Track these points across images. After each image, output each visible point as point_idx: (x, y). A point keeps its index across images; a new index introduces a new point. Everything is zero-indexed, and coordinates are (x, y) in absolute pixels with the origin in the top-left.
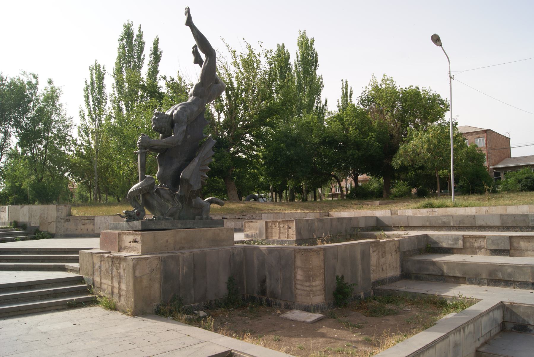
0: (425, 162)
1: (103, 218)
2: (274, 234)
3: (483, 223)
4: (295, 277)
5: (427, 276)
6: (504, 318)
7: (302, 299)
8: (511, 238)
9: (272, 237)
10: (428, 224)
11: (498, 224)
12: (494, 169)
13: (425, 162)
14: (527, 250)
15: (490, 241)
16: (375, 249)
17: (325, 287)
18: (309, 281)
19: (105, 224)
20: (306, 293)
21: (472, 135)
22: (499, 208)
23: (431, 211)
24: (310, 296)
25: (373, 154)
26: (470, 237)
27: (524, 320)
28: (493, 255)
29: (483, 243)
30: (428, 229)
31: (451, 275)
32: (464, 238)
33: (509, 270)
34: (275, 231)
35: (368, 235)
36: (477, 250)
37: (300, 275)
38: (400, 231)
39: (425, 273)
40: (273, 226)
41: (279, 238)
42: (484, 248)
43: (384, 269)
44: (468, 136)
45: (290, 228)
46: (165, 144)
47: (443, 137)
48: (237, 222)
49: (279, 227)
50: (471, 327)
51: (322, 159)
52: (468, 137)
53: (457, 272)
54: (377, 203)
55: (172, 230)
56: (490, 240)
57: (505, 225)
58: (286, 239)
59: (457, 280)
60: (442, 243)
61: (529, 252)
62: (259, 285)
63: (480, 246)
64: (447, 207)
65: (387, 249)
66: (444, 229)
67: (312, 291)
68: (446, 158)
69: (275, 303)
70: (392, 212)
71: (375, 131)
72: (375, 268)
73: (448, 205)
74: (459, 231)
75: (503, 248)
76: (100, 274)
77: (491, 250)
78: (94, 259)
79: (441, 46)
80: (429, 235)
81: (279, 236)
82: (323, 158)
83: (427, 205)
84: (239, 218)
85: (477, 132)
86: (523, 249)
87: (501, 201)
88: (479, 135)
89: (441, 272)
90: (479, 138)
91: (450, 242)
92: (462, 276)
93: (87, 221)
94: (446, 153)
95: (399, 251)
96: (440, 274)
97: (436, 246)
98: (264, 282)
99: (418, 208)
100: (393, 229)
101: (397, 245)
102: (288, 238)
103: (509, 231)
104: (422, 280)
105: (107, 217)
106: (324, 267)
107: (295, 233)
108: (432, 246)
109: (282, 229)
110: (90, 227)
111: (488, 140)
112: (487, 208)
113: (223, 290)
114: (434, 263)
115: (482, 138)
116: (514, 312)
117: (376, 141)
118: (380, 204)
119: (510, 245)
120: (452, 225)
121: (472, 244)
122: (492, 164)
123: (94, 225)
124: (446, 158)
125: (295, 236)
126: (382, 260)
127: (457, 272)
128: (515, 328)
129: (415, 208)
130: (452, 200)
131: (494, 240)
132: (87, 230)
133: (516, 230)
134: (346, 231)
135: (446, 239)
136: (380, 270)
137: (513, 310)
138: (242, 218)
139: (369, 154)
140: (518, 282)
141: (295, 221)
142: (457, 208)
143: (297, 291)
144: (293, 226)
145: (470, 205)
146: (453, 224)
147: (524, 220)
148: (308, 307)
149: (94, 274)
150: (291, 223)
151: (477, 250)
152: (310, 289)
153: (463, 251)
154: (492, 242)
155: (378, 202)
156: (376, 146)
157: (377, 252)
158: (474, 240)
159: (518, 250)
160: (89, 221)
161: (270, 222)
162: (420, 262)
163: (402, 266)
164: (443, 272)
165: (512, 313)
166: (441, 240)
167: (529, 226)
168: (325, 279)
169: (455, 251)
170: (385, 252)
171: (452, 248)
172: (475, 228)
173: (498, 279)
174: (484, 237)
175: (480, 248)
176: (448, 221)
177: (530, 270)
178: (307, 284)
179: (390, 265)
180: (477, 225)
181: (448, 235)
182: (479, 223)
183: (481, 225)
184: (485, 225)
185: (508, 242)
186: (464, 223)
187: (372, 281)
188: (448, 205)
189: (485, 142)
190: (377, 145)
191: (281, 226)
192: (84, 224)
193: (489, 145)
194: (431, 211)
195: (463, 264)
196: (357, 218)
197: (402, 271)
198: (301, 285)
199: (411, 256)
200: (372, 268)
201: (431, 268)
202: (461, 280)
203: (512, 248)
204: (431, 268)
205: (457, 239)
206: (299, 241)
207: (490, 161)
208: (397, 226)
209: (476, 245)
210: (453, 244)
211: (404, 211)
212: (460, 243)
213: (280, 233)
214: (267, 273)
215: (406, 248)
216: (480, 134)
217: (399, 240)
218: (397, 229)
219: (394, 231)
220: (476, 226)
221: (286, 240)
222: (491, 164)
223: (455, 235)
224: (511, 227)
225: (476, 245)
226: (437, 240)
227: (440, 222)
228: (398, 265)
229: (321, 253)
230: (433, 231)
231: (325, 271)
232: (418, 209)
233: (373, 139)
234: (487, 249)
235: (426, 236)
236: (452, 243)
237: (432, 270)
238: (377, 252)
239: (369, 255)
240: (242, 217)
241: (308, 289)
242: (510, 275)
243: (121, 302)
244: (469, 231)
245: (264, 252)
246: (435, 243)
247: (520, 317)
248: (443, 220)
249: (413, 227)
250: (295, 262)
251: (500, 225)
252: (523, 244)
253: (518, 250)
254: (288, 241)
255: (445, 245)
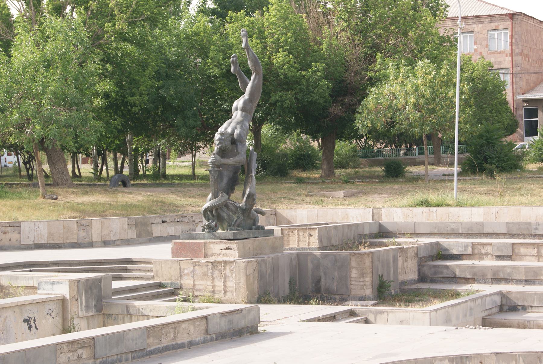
0: (410, 125)
1: (32, 225)
2: (291, 242)
3: (490, 231)
4: (351, 275)
5: (442, 279)
6: (502, 302)
7: (355, 291)
8: (513, 244)
9: (288, 245)
10: (436, 231)
11: (504, 231)
12: (525, 101)
13: (410, 125)
14: (526, 256)
15: (496, 248)
16: (401, 254)
17: (372, 282)
18: (363, 277)
19: (35, 231)
20: (360, 287)
21: (482, 23)
22: (512, 209)
23: (428, 211)
24: (364, 289)
25: (318, 101)
26: (479, 244)
27: (515, 303)
28: (498, 260)
29: (489, 249)
30: (436, 237)
31: (462, 276)
32: (473, 245)
33: (509, 270)
34: (293, 239)
35: (376, 242)
36: (484, 256)
37: (354, 273)
38: (405, 238)
39: (440, 276)
40: (290, 233)
41: (298, 246)
42: (490, 254)
43: (407, 272)
44: (474, 23)
45: (311, 235)
46: (234, 163)
47: (438, 82)
48: (177, 227)
49: (298, 234)
50: (480, 300)
51: (216, 102)
52: (474, 26)
53: (467, 274)
54: (341, 194)
55: (252, 239)
56: (496, 247)
57: (510, 233)
58: (307, 247)
59: (467, 280)
60: (452, 250)
61: (527, 257)
62: (314, 285)
63: (487, 252)
64: (448, 205)
65: (409, 254)
66: (452, 236)
67: (365, 285)
68: (442, 119)
69: (330, 298)
70: (374, 211)
71: (322, 59)
72: (400, 270)
73: (450, 203)
74: (468, 238)
75: (506, 254)
76: (193, 277)
77: (496, 256)
78: (181, 265)
79: (497, 313)
80: (441, 243)
81: (298, 244)
82: (218, 99)
83: (422, 202)
84: (178, 221)
85: (494, 16)
86: (522, 254)
87: (517, 198)
88: (496, 24)
89: (454, 275)
90: (498, 29)
91: (460, 249)
92: (471, 277)
93: (9, 229)
94: (442, 111)
95: (417, 257)
96: (452, 276)
97: (446, 253)
98: (319, 281)
99: (410, 206)
100: (398, 235)
101: (416, 251)
102: (308, 245)
103: (514, 238)
104: (436, 283)
105: (38, 223)
106: (372, 267)
107: (317, 241)
108: (443, 253)
109: (301, 237)
110: (14, 236)
111: (516, 36)
112: (497, 209)
113: (287, 291)
114: (447, 267)
115: (503, 32)
116: (509, 298)
117: (324, 78)
118: (344, 196)
119: (512, 251)
120: (460, 232)
121: (480, 251)
122: (521, 89)
123: (19, 233)
124: (442, 119)
125: (317, 244)
126: (405, 264)
127: (467, 274)
128: (509, 309)
129: (405, 207)
130: (455, 196)
131: (500, 247)
132: (10, 240)
133: (521, 237)
134: (354, 238)
135: (456, 246)
136: (404, 272)
137: (508, 296)
138: (181, 221)
139: (309, 100)
140: (515, 279)
141: (317, 229)
142: (462, 209)
143: (351, 286)
144: (316, 234)
145: (476, 204)
146: (462, 231)
147: (528, 228)
148: (362, 297)
149: (181, 278)
150: (313, 231)
151: (484, 256)
152: (364, 283)
153: (472, 257)
154: (498, 248)
155: (342, 192)
156: (323, 86)
157: (402, 257)
158: (482, 247)
159: (518, 255)
160: (12, 228)
161: (286, 229)
162: (435, 266)
163: (419, 270)
164: (455, 275)
165: (508, 298)
166: (452, 247)
167: (531, 234)
168: (372, 276)
169: (464, 257)
170: (407, 257)
171: (462, 255)
172: (483, 235)
173: (499, 278)
174: (490, 244)
175: (487, 254)
176: (456, 227)
177: (523, 270)
178: (362, 280)
179: (410, 269)
180: (485, 232)
181: (459, 242)
182: (487, 230)
183: (489, 232)
184: (493, 232)
185: (511, 248)
186: (472, 230)
187: (399, 281)
188: (450, 202)
189: (509, 40)
190: (326, 84)
191: (301, 233)
192: (5, 233)
193: (518, 48)
194: (428, 211)
195: (473, 267)
196: (363, 223)
197: (419, 275)
198: (355, 281)
199: (426, 262)
200: (399, 270)
201: (445, 271)
202: (470, 280)
203: (514, 254)
204: (445, 271)
205: (466, 246)
206: (321, 248)
207: (516, 82)
208: (403, 232)
209: (483, 251)
210: (463, 251)
211: (391, 210)
212: (469, 250)
213: (299, 241)
214: (322, 274)
215: (422, 254)
216: (498, 20)
217: (417, 247)
218: (402, 236)
219: (399, 238)
220: (484, 234)
221: (307, 248)
222: (519, 90)
223: (465, 242)
224: (516, 234)
225: (483, 251)
226: (448, 247)
227: (449, 229)
228: (416, 269)
229: (370, 256)
230: (441, 238)
231: (372, 270)
232: (411, 208)
233: (319, 74)
234: (493, 255)
235: (438, 243)
236: (462, 249)
237: (446, 273)
238: (402, 257)
239: (398, 260)
240: (182, 219)
241: (362, 283)
242: (509, 274)
243: (227, 297)
244: (477, 238)
245: (319, 257)
246: (446, 250)
247: (513, 301)
248: (452, 227)
249: (420, 233)
250: (350, 263)
251: (506, 232)
252: (523, 250)
253: (518, 255)
254: (309, 248)
255: (455, 252)
